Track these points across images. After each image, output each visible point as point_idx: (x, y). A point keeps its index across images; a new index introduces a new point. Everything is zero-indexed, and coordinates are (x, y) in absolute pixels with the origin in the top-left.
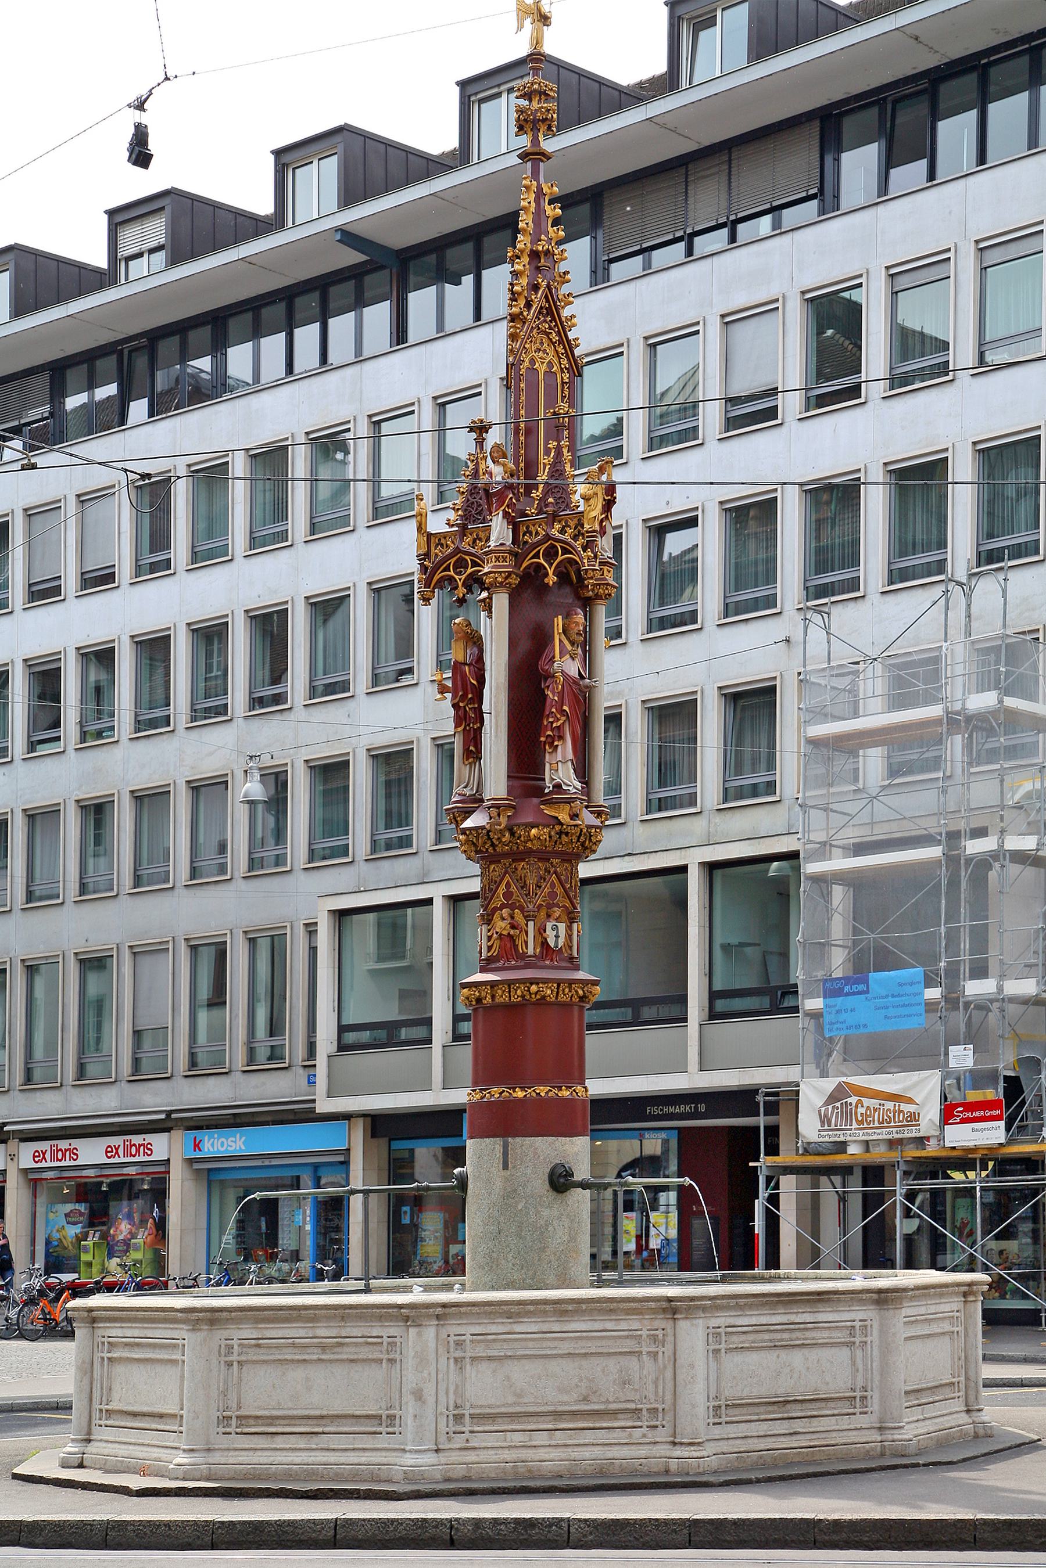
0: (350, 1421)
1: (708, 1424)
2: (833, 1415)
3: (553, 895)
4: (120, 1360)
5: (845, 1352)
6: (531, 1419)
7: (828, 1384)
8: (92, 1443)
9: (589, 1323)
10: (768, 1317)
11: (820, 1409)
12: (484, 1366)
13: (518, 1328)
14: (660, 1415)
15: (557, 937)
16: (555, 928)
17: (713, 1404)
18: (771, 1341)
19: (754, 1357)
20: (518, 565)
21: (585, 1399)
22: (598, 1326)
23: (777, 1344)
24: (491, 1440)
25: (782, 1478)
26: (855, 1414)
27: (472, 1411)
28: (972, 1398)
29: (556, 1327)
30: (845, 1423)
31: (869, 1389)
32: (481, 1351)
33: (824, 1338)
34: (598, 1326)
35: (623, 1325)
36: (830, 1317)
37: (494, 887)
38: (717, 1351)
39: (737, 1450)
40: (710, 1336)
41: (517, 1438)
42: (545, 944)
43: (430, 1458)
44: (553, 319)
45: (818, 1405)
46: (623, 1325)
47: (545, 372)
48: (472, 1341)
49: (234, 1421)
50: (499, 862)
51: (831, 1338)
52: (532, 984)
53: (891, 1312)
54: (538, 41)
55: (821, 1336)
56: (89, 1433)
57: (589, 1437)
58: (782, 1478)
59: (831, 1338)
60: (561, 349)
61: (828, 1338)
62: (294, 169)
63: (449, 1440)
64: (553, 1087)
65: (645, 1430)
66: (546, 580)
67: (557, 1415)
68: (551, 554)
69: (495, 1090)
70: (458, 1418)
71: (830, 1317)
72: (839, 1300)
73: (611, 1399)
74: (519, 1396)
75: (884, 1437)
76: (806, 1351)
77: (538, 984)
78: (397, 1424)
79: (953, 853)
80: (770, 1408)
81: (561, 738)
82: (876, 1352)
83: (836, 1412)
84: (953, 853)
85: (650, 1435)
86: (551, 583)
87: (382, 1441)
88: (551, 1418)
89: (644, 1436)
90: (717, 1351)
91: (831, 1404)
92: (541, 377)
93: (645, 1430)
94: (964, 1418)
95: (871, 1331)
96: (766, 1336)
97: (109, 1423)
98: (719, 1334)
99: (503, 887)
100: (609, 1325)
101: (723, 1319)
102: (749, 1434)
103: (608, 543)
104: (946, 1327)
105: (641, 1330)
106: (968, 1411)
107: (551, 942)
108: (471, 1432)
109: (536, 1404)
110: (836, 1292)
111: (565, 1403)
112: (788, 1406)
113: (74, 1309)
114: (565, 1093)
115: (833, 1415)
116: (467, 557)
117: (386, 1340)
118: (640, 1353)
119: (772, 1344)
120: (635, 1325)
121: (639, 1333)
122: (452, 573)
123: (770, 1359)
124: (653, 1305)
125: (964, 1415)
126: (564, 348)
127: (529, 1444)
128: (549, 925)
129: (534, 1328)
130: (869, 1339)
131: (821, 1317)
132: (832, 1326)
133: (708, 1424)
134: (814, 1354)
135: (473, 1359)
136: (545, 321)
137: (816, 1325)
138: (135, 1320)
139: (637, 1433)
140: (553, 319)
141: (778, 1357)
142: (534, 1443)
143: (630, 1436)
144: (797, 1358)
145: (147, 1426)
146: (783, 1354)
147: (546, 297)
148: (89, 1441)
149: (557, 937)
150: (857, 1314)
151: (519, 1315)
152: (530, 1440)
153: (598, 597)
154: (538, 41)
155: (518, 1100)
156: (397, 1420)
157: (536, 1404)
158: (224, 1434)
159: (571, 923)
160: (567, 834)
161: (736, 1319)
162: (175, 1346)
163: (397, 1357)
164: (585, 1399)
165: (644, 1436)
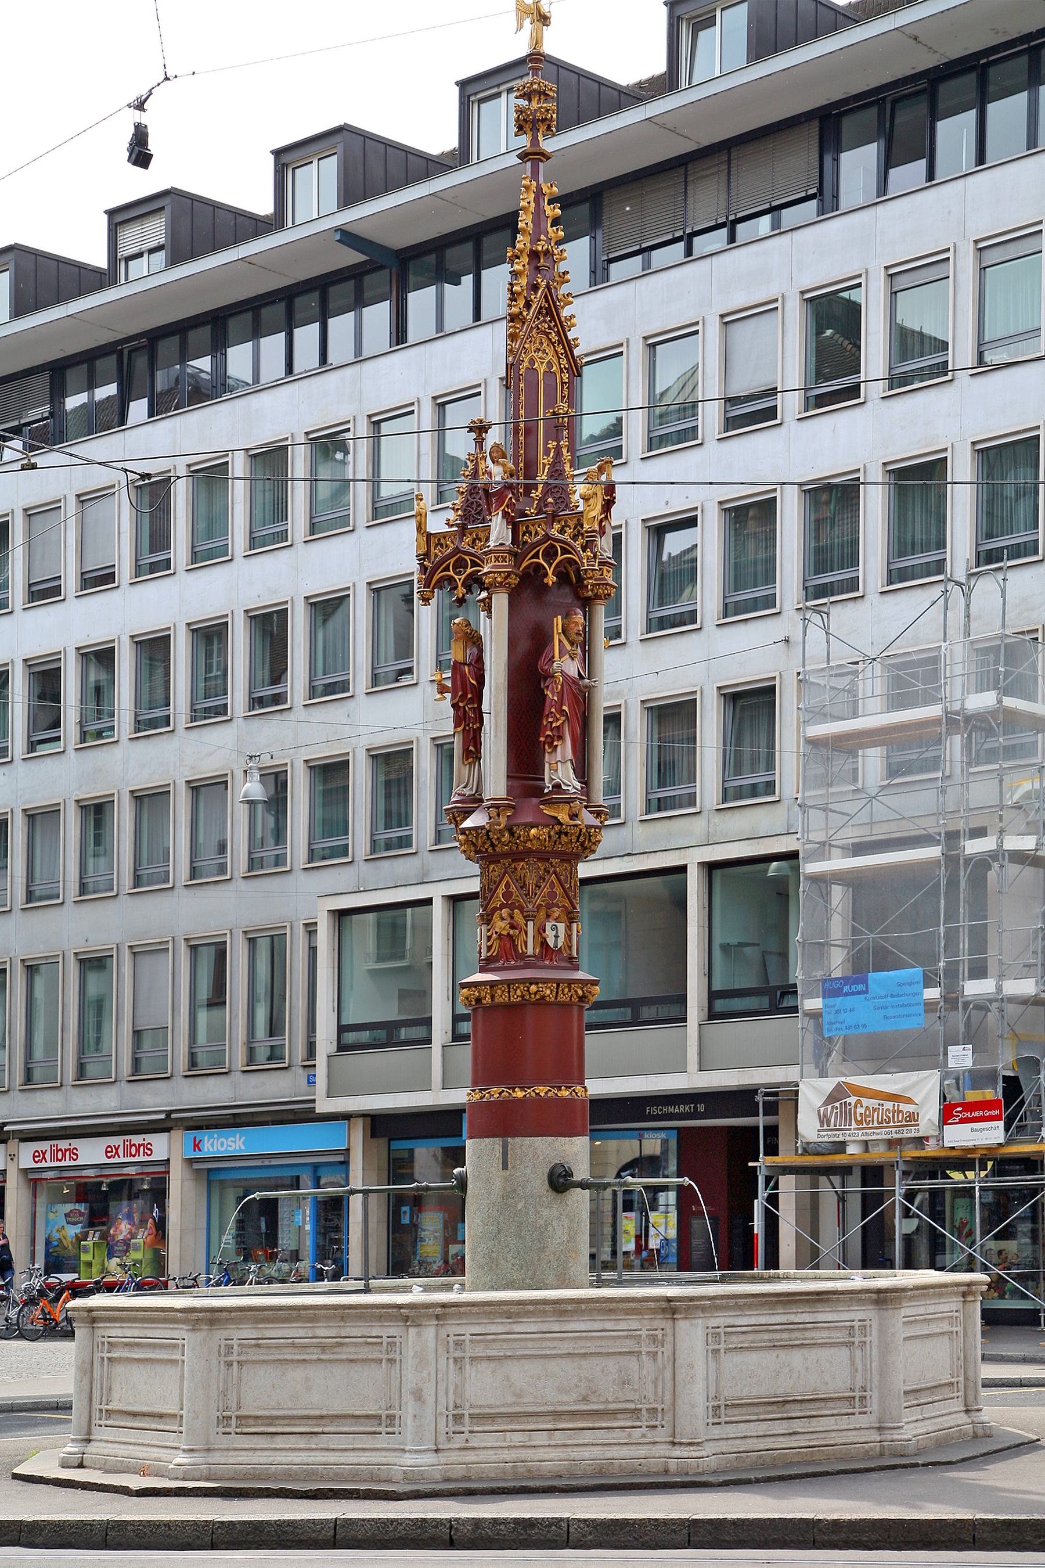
0: (349, 1421)
1: (708, 1424)
2: (833, 1415)
3: (552, 895)
4: (120, 1360)
5: (845, 1352)
6: (530, 1419)
7: (827, 1384)
8: (92, 1443)
9: (589, 1323)
10: (768, 1317)
11: (819, 1409)
12: (484, 1366)
13: (517, 1328)
14: (660, 1415)
15: (556, 937)
16: (555, 928)
17: (712, 1404)
18: (770, 1341)
19: (753, 1357)
20: (517, 565)
21: (585, 1399)
22: (597, 1326)
23: (776, 1344)
24: (491, 1440)
25: (782, 1478)
26: (854, 1414)
27: (472, 1411)
28: (971, 1398)
29: (556, 1327)
30: (844, 1423)
31: (868, 1389)
32: (480, 1351)
33: (823, 1338)
34: (597, 1326)
35: (623, 1325)
36: (830, 1317)
37: (493, 887)
38: (716, 1351)
39: (736, 1450)
40: (710, 1336)
41: (517, 1438)
42: (544, 944)
43: (430, 1458)
44: (553, 319)
45: (817, 1405)
46: (623, 1325)
47: (545, 372)
48: (471, 1341)
49: (234, 1421)
50: (499, 862)
51: (830, 1338)
52: (531, 984)
53: (890, 1312)
54: (537, 41)
55: (821, 1336)
56: (89, 1433)
57: (588, 1437)
58: (782, 1478)
59: (830, 1338)
60: (560, 349)
61: (827, 1338)
62: (294, 169)
63: (449, 1440)
64: (553, 1087)
65: (644, 1430)
66: (546, 580)
67: (557, 1415)
68: (550, 554)
69: (495, 1090)
70: (458, 1418)
71: (830, 1317)
72: (838, 1300)
73: (610, 1399)
74: (519, 1396)
75: (883, 1437)
76: (805, 1351)
77: (537, 984)
78: (397, 1424)
79: (952, 853)
80: (770, 1408)
81: (560, 738)
82: (875, 1352)
83: (835, 1412)
84: (952, 853)
85: (649, 1435)
86: (551, 583)
87: (381, 1441)
88: (550, 1418)
89: (644, 1436)
90: (716, 1351)
91: (831, 1404)
92: (541, 377)
93: (644, 1430)
94: (963, 1418)
95: (871, 1331)
96: (766, 1336)
97: (108, 1423)
98: (718, 1334)
99: (502, 887)
100: (609, 1325)
101: (723, 1319)
102: (748, 1434)
103: (608, 543)
104: (945, 1327)
105: (641, 1330)
106: (967, 1411)
107: (551, 942)
108: (471, 1432)
109: (536, 1404)
110: (835, 1292)
111: (564, 1403)
112: (788, 1406)
113: (74, 1309)
114: (565, 1093)
115: (833, 1415)
116: (466, 557)
117: (385, 1340)
118: (639, 1353)
119: (771, 1344)
120: (635, 1325)
121: (639, 1333)
122: (451, 573)
123: (769, 1359)
124: (652, 1305)
125: (963, 1415)
126: (564, 348)
127: (528, 1444)
128: (548, 925)
129: (533, 1328)
130: (868, 1339)
131: (820, 1317)
132: (831, 1326)
133: (708, 1424)
134: (813, 1354)
135: (473, 1359)
136: (545, 321)
137: (815, 1325)
138: (135, 1320)
139: (637, 1433)
140: (553, 319)
141: (777, 1357)
142: (533, 1443)
143: (630, 1436)
144: (796, 1358)
145: (147, 1426)
146: (782, 1354)
147: (546, 297)
148: (89, 1441)
149: (556, 937)
150: (856, 1314)
151: (518, 1315)
152: (530, 1440)
153: (597, 597)
154: (537, 41)
155: (517, 1100)
156: (397, 1420)
157: (536, 1404)
158: (223, 1434)
159: (571, 923)
160: (566, 834)
161: (735, 1319)
162: (175, 1346)
163: (397, 1357)
164: (585, 1399)
165: (644, 1436)
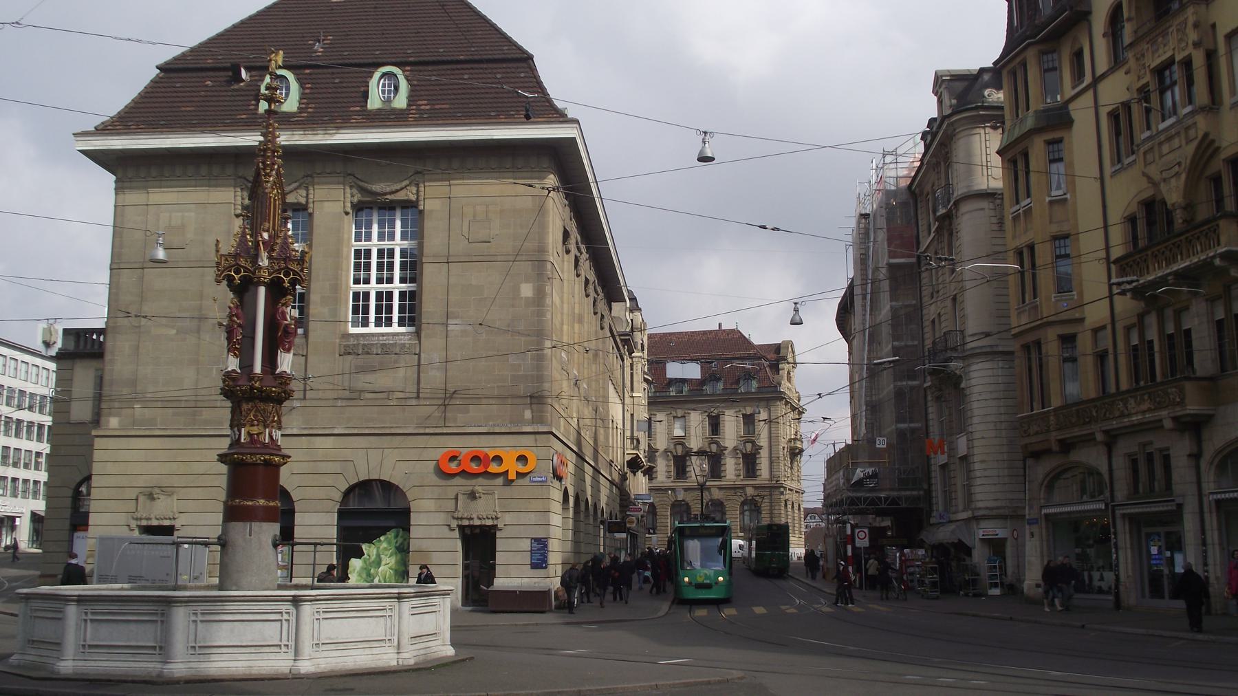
20: (269, 275)
90: (86, 621)
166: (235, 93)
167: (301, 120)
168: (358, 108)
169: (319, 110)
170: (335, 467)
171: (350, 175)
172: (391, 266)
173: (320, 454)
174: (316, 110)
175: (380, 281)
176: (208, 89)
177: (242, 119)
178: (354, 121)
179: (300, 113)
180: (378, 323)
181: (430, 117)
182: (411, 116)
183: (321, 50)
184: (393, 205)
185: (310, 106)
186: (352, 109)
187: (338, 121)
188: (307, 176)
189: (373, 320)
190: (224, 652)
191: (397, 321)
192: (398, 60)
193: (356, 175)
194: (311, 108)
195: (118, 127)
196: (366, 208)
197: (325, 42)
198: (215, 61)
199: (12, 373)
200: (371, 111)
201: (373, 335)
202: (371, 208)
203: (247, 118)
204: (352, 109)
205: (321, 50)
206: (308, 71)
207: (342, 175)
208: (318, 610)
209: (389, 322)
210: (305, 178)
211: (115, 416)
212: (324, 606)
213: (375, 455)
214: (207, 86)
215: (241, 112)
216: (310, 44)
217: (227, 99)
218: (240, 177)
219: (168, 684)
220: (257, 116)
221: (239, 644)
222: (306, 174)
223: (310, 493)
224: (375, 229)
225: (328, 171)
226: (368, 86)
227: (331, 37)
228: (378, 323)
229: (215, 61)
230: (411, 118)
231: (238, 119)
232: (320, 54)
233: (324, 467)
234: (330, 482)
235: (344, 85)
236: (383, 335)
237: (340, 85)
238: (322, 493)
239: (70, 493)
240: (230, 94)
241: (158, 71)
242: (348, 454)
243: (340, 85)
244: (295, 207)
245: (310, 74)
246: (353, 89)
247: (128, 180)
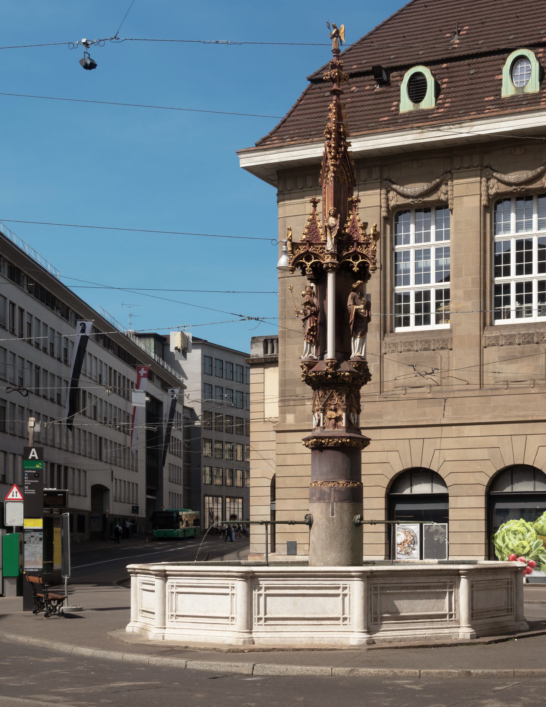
166: (378, 96)
167: (438, 116)
168: (492, 98)
169: (455, 104)
170: (484, 454)
171: (487, 167)
172: (529, 256)
173: (470, 442)
174: (452, 104)
175: (519, 271)
176: (354, 95)
177: (385, 121)
178: (488, 111)
179: (437, 109)
180: (418, 322)
181: (529, 103)
182: (543, 99)
183: (458, 41)
184: (530, 194)
185: (447, 100)
186: (486, 99)
187: (472, 113)
188: (446, 173)
189: (533, 312)
190: (288, 624)
191: (511, 312)
192: (532, 42)
193: (492, 167)
194: (447, 103)
195: (275, 142)
196: (505, 200)
197: (461, 33)
198: (360, 66)
199: (229, 376)
200: (504, 99)
201: (514, 326)
202: (409, 211)
203: (388, 120)
204: (486, 99)
205: (458, 41)
206: (445, 65)
207: (479, 168)
208: (172, 584)
209: (427, 321)
210: (445, 175)
211: (290, 412)
212: (382, 581)
213: (519, 441)
214: (352, 92)
215: (383, 115)
216: (448, 37)
217: (371, 102)
218: (386, 180)
219: (414, 648)
220: (398, 117)
221: (301, 616)
222: (445, 171)
223: (463, 478)
224: (433, 229)
225: (466, 165)
226: (399, 90)
227: (467, 27)
228: (418, 322)
229: (360, 66)
230: (543, 101)
231: (381, 121)
232: (456, 46)
233: (472, 454)
234: (478, 468)
235: (480, 75)
236: (423, 332)
237: (476, 76)
238: (472, 479)
239: (269, 483)
240: (373, 97)
241: (309, 83)
242: (493, 441)
243: (476, 76)
244: (438, 205)
245: (447, 68)
246: (487, 79)
247: (363, 182)
